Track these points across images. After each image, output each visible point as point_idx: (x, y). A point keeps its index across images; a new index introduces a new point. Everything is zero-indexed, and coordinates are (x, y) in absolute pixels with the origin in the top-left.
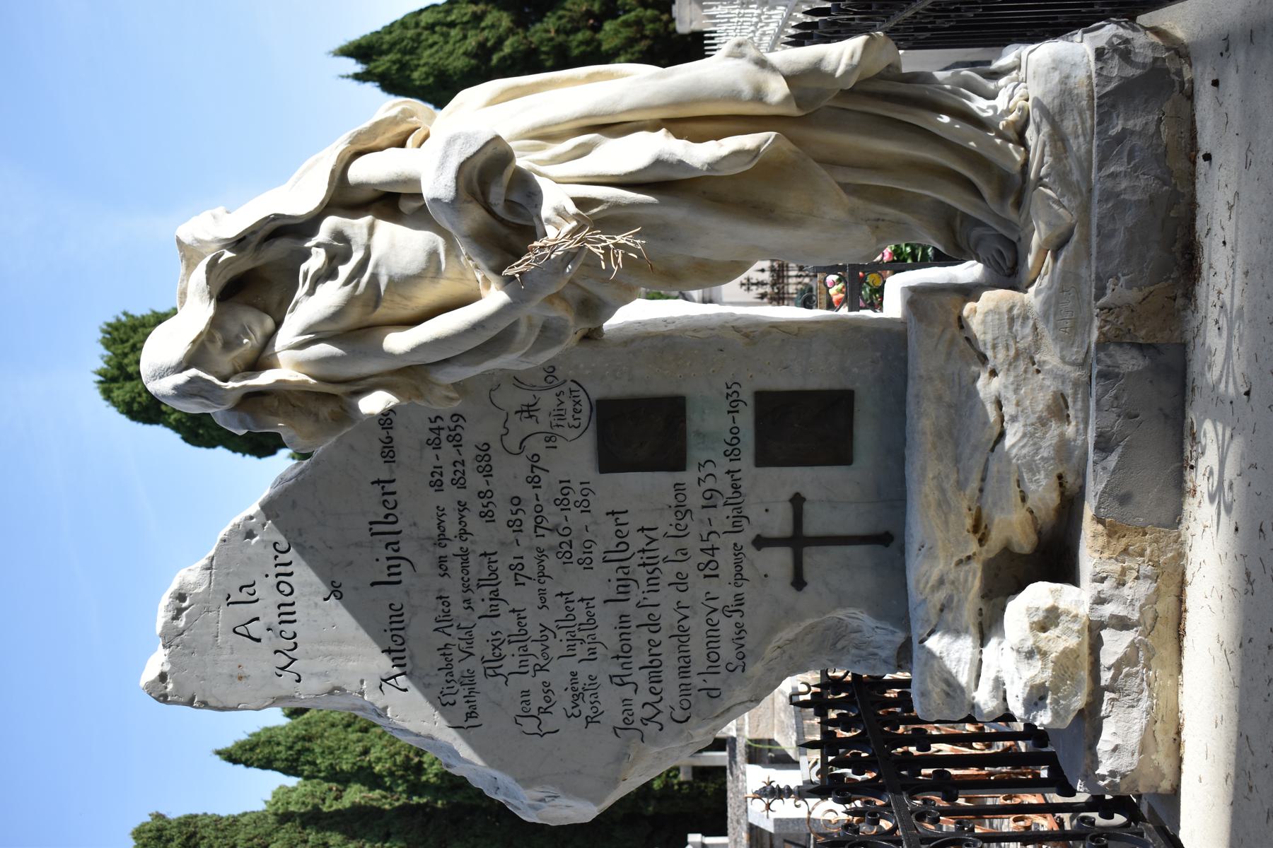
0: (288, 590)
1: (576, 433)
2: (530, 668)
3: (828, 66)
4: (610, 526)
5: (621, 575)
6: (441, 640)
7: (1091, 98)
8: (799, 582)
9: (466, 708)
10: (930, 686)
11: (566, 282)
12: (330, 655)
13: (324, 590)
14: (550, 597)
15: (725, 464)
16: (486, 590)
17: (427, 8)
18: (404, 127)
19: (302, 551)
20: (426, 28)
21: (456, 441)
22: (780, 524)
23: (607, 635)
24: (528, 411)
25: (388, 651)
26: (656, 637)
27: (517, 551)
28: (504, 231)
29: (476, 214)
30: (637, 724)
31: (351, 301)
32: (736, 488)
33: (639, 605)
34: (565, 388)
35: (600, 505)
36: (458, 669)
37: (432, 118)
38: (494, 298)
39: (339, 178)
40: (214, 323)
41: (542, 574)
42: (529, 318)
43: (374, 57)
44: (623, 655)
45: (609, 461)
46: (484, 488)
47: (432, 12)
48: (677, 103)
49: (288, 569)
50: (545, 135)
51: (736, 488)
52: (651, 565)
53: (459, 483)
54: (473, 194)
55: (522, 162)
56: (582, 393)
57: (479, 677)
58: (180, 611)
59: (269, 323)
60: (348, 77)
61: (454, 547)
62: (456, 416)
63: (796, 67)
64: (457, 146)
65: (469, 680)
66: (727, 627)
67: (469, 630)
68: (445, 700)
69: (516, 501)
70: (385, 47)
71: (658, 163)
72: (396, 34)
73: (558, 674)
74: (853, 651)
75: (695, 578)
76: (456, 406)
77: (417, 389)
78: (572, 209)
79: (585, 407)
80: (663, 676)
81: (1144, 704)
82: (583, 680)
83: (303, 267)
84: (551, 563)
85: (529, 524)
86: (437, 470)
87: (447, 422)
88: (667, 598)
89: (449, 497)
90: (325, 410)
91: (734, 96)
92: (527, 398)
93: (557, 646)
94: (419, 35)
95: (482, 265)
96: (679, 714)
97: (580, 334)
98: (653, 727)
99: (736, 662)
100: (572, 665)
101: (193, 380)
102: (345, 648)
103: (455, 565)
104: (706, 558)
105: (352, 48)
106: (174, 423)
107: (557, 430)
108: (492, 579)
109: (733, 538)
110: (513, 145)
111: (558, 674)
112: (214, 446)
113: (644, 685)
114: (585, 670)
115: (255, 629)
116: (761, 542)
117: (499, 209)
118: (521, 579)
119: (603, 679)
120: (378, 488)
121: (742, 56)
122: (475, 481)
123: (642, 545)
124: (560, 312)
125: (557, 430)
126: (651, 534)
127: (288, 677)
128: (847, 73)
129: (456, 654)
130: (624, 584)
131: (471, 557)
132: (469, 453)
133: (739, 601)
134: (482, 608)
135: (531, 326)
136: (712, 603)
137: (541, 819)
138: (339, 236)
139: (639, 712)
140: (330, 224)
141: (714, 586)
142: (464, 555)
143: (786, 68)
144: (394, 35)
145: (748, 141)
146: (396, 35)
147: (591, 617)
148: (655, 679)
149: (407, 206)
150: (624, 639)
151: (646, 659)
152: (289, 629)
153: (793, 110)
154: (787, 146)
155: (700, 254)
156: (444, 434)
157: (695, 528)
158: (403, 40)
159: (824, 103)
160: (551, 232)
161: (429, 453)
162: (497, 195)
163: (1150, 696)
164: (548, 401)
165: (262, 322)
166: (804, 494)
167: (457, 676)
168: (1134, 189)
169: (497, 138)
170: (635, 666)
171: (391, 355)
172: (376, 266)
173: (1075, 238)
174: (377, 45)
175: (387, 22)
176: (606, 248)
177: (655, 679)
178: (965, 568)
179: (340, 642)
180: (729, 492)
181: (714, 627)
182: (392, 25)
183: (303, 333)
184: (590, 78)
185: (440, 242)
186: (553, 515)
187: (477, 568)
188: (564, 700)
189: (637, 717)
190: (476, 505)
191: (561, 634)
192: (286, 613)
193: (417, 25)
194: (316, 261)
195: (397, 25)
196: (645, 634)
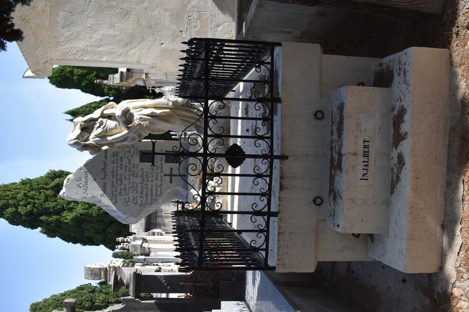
0: (87, 179)
1: (136, 156)
2: (126, 194)
3: (178, 101)
4: (141, 171)
5: (142, 179)
6: (112, 189)
7: (216, 108)
8: (171, 182)
9: (115, 201)
10: (190, 197)
11: (136, 130)
12: (93, 190)
13: (93, 179)
14: (131, 183)
15: (160, 162)
16: (120, 181)
17: (93, 102)
18: (113, 106)
19: (90, 173)
20: (93, 108)
21: (117, 156)
22: (168, 172)
23: (139, 189)
24: (129, 152)
25: (103, 190)
26: (147, 190)
27: (126, 174)
28: (128, 122)
29: (124, 118)
30: (143, 205)
31: (103, 131)
32: (162, 166)
33: (145, 185)
34: (135, 148)
35: (140, 167)
36: (114, 194)
37: (117, 106)
38: (126, 132)
39: (102, 113)
40: (80, 133)
41: (129, 179)
42: (131, 136)
43: (77, 115)
44: (142, 193)
45: (142, 161)
46: (121, 164)
47: (95, 103)
48: (155, 105)
49: (87, 176)
50: (135, 108)
51: (162, 166)
52: (147, 178)
53: (117, 163)
54: (124, 115)
55: (131, 111)
56: (138, 149)
57: (118, 195)
58: (68, 182)
59: (89, 135)
60: (68, 120)
61: (115, 173)
62: (117, 152)
63: (174, 101)
64: (122, 108)
65: (116, 196)
66: (159, 189)
67: (117, 187)
68: (112, 199)
69: (126, 166)
70: (80, 112)
71: (152, 113)
72: (84, 109)
73: (131, 196)
74: (180, 196)
75: (154, 180)
76: (118, 150)
77: (112, 146)
78: (139, 118)
79: (138, 151)
80: (148, 197)
81: (222, 199)
82: (135, 197)
83: (95, 126)
84: (131, 177)
85: (128, 170)
86: (114, 161)
87: (116, 153)
88: (150, 183)
89: (115, 165)
90: (96, 149)
91: (164, 104)
92: (129, 150)
93: (131, 191)
94: (91, 110)
95: (124, 127)
96: (150, 203)
97: (138, 140)
98: (146, 205)
99: (160, 195)
100: (133, 194)
101: (77, 142)
102: (96, 189)
103: (115, 176)
104: (156, 177)
105: (70, 112)
106: (7, 217)
107: (134, 155)
108: (121, 179)
109: (161, 174)
110: (130, 109)
111: (131, 196)
112: (18, 225)
113: (145, 198)
114: (135, 195)
115: (80, 185)
116: (165, 175)
117: (127, 118)
118: (126, 179)
119: (138, 197)
120: (103, 163)
121: (166, 99)
122: (120, 163)
123: (146, 175)
124: (135, 135)
125: (134, 155)
126: (148, 173)
127: (85, 194)
128: (181, 102)
129: (114, 191)
130: (143, 181)
131: (118, 175)
132: (119, 158)
133: (161, 185)
134: (119, 184)
135: (131, 138)
136: (157, 185)
137: (127, 223)
138: (102, 121)
139: (144, 203)
140: (100, 119)
141: (157, 182)
142: (117, 175)
143: (172, 101)
144: (83, 109)
145: (166, 110)
146: (84, 109)
147: (137, 186)
148: (147, 197)
149: (112, 118)
150: (142, 190)
151: (145, 194)
152: (86, 186)
153: (173, 107)
154: (172, 112)
155: (158, 127)
156: (115, 155)
157: (155, 172)
158: (86, 111)
159: (178, 107)
160: (135, 121)
161: (113, 157)
162: (127, 116)
163: (223, 198)
164: (132, 150)
165: (87, 134)
166: (172, 168)
167: (114, 195)
168: (221, 121)
169: (128, 107)
170: (144, 195)
171: (108, 140)
172: (107, 126)
173: (213, 128)
174: (78, 112)
175: (81, 105)
176: (144, 124)
177: (147, 197)
178: (196, 179)
179: (95, 188)
180: (160, 167)
181: (157, 189)
182: (83, 106)
183: (94, 136)
184: (143, 101)
185: (117, 123)
186: (132, 169)
187: (119, 177)
188: (132, 200)
189: (143, 203)
190: (119, 167)
191: (132, 189)
192: (86, 183)
193: (90, 107)
194: (98, 125)
195: (84, 107)
196: (146, 189)
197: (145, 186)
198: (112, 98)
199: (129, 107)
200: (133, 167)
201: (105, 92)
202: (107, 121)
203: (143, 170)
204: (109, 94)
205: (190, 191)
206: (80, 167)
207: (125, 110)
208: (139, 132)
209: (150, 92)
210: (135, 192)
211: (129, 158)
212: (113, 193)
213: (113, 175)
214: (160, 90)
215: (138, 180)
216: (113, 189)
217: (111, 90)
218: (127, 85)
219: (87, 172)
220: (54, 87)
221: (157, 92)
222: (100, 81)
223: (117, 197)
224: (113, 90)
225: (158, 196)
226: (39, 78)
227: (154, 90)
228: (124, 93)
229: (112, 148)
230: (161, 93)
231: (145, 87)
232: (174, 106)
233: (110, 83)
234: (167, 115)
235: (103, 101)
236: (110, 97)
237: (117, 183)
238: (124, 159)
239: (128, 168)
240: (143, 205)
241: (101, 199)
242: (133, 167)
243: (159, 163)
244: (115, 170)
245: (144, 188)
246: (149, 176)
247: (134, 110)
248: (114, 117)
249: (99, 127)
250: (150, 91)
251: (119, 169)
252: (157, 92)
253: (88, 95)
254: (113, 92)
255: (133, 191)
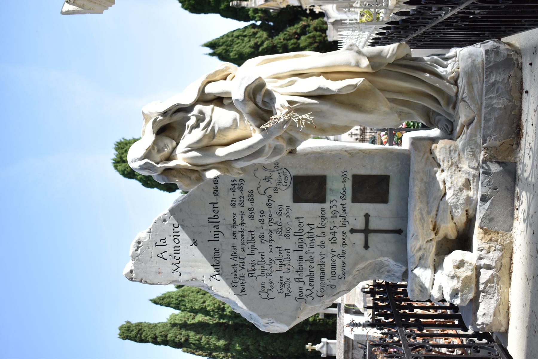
0: (177, 242)
1: (285, 187)
2: (265, 274)
4: (296, 223)
5: (300, 241)
6: (233, 262)
8: (366, 247)
10: (415, 288)
12: (192, 266)
13: (191, 242)
15: (340, 201)
17: (236, 30)
18: (226, 73)
19: (183, 227)
20: (236, 37)
21: (241, 189)
22: (360, 224)
23: (294, 263)
24: (268, 179)
25: (213, 266)
27: (262, 231)
28: (261, 112)
29: (251, 106)
30: (304, 297)
31: (204, 136)
32: (344, 210)
34: (282, 171)
35: (294, 214)
36: (239, 273)
38: (257, 136)
39: (202, 91)
40: (155, 143)
41: (271, 240)
44: (300, 271)
45: (297, 198)
47: (238, 31)
49: (178, 234)
51: (344, 210)
52: (311, 238)
53: (242, 204)
54: (250, 98)
56: (288, 173)
57: (246, 277)
58: (138, 248)
59: (174, 143)
60: (207, 54)
61: (239, 228)
62: (241, 180)
63: (372, 54)
65: (242, 278)
66: (339, 262)
68: (233, 284)
69: (262, 212)
70: (220, 44)
73: (276, 277)
74: (386, 273)
76: (241, 176)
77: (227, 169)
80: (315, 279)
81: (496, 298)
82: (284, 279)
83: (187, 123)
84: (275, 236)
85: (267, 221)
86: (234, 200)
87: (238, 182)
88: (317, 250)
89: (238, 210)
90: (194, 176)
92: (267, 174)
93: (275, 267)
94: (233, 39)
95: (253, 124)
96: (320, 294)
97: (288, 151)
98: (310, 298)
99: (342, 275)
100: (280, 273)
101: (146, 163)
102: (197, 264)
103: (239, 235)
104: (332, 236)
105: (208, 44)
107: (278, 186)
109: (343, 229)
111: (276, 277)
112: (153, 188)
113: (307, 282)
114: (285, 276)
115: (165, 255)
116: (352, 231)
117: (260, 104)
118: (263, 241)
119: (292, 280)
120: (212, 205)
121: (352, 50)
122: (247, 204)
123: (308, 230)
124: (281, 143)
125: (278, 186)
126: (312, 226)
127: (176, 274)
128: (390, 57)
129: (238, 268)
130: (301, 245)
131: (245, 232)
132: (246, 194)
133: (344, 252)
134: (248, 251)
135: (270, 147)
136: (334, 253)
137: (267, 330)
139: (305, 293)
141: (334, 247)
142: (242, 231)
143: (368, 54)
149: (226, 102)
150: (300, 265)
151: (308, 273)
152: (177, 256)
153: (370, 70)
154: (368, 83)
157: (328, 225)
161: (231, 193)
163: (498, 295)
164: (275, 175)
165: (172, 143)
167: (238, 276)
170: (304, 275)
172: (214, 124)
173: (475, 121)
175: (222, 35)
176: (299, 120)
178: (429, 244)
180: (341, 212)
181: (334, 262)
182: (223, 36)
184: (295, 56)
185: (237, 116)
186: (276, 218)
188: (277, 287)
190: (247, 213)
191: (277, 262)
192: (177, 250)
193: (232, 36)
194: (192, 121)
197: (307, 257)
198: (259, 23)
199: (263, 78)
200: (279, 213)
201: (250, 15)
202: (213, 110)
203: (301, 220)
204: (255, 18)
205: (414, 272)
206: (161, 214)
207: (254, 85)
208: (288, 133)
209: (307, 13)
210: (284, 269)
211: (267, 194)
212: (235, 271)
213: (234, 233)
214: (321, 9)
215: (291, 243)
216: (235, 262)
217: (257, 13)
218: (275, 5)
219: (176, 225)
220: (187, 12)
221: (317, 12)
222: (237, 3)
223: (246, 281)
224: (259, 12)
225: (336, 278)
226: (91, 13)
227: (313, 9)
228: (274, 15)
229: (229, 172)
230: (322, 12)
231: (301, 7)
232: (373, 69)
233: (251, 5)
234: (359, 91)
235: (248, 27)
236: (256, 21)
237: (243, 250)
238: (256, 196)
239: (267, 215)
240: (304, 297)
241: (209, 285)
242: (279, 213)
243: (338, 204)
244: (238, 221)
245: (304, 259)
246: (315, 234)
247: (275, 82)
248: (229, 101)
249: (197, 126)
250: (308, 12)
251: (246, 219)
252: (317, 12)
253: (229, 20)
254: (260, 14)
255: (280, 267)
